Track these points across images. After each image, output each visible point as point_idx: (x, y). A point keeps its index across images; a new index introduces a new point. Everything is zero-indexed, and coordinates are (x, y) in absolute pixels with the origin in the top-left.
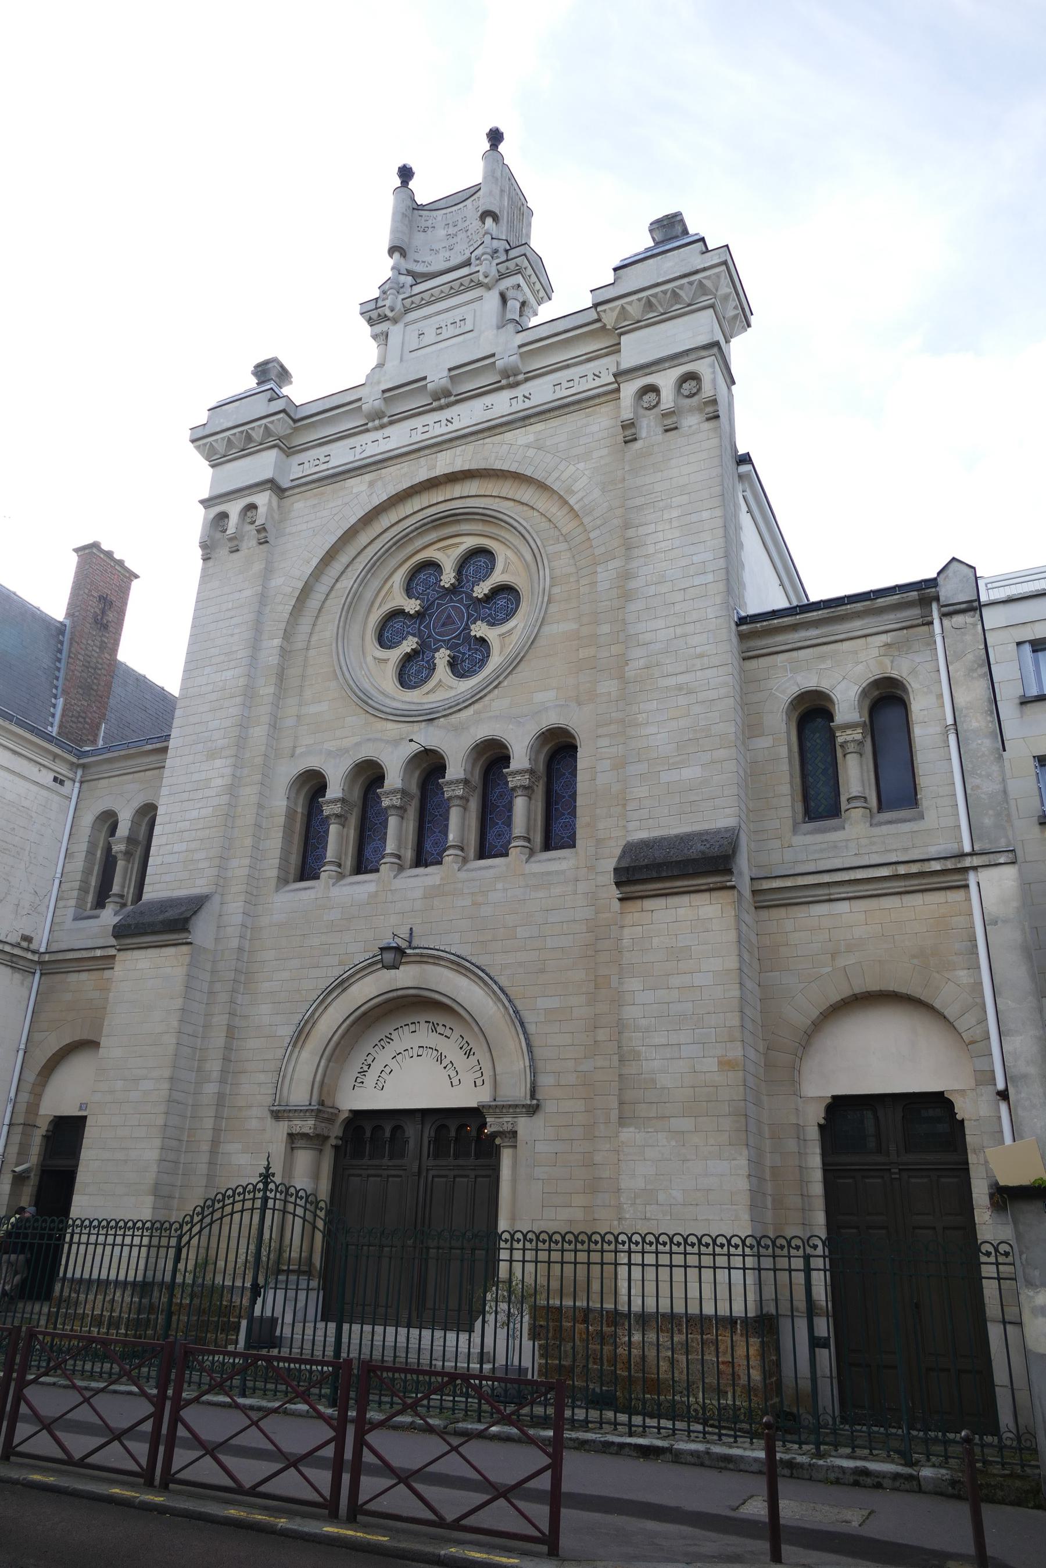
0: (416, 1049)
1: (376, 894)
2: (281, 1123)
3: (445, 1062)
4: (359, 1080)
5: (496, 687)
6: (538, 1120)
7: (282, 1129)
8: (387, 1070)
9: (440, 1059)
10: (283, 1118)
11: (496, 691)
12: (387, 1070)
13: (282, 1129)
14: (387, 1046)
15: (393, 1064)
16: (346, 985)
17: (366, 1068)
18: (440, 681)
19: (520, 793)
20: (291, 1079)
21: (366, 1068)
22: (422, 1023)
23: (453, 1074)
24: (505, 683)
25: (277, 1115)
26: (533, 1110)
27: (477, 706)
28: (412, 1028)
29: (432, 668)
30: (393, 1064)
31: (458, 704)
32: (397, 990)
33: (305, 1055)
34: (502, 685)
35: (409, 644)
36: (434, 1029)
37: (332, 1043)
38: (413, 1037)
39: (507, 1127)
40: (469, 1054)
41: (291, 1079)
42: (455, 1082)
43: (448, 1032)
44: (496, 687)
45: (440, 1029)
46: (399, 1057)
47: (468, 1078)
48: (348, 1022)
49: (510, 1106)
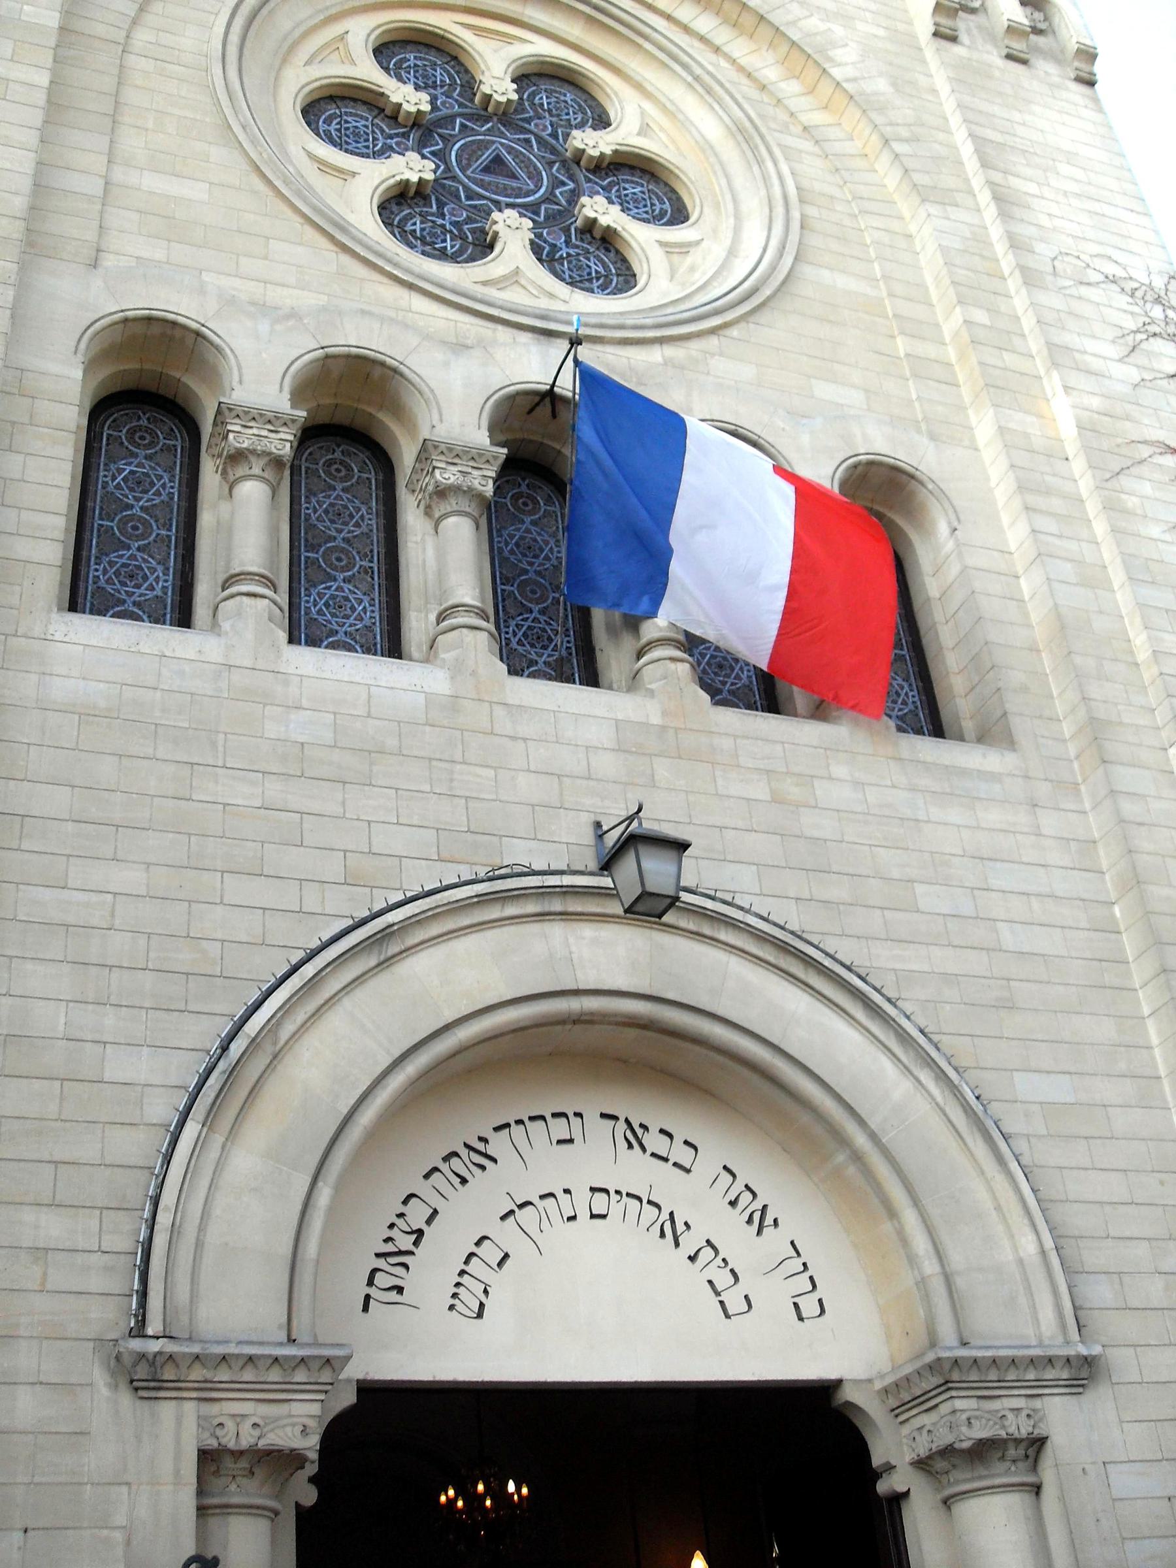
0: (582, 1196)
1: (453, 703)
2: (167, 1410)
3: (691, 1242)
4: (381, 1280)
5: (713, 331)
6: (1099, 1402)
7: (176, 1431)
8: (491, 1254)
9: (672, 1230)
10: (177, 1385)
11: (714, 341)
12: (491, 1254)
13: (176, 1431)
14: (477, 1179)
15: (507, 1236)
16: (393, 949)
17: (406, 1242)
18: (354, 174)
19: (256, 470)
20: (199, 1245)
21: (406, 1242)
22: (592, 1117)
23: (723, 1280)
24: (734, 332)
25: (147, 1378)
26: (1083, 1373)
27: (670, 351)
28: (559, 1129)
29: (383, 152)
30: (507, 1236)
31: (622, 327)
32: (577, 993)
33: (246, 1160)
34: (728, 332)
35: (410, 98)
36: (635, 1138)
37: (356, 1133)
38: (574, 1155)
39: (1020, 1427)
40: (760, 1221)
41: (199, 1245)
42: (735, 1304)
43: (683, 1155)
44: (713, 331)
45: (655, 1142)
46: (522, 1215)
47: (775, 1295)
48: (411, 1069)
49: (1032, 1361)
